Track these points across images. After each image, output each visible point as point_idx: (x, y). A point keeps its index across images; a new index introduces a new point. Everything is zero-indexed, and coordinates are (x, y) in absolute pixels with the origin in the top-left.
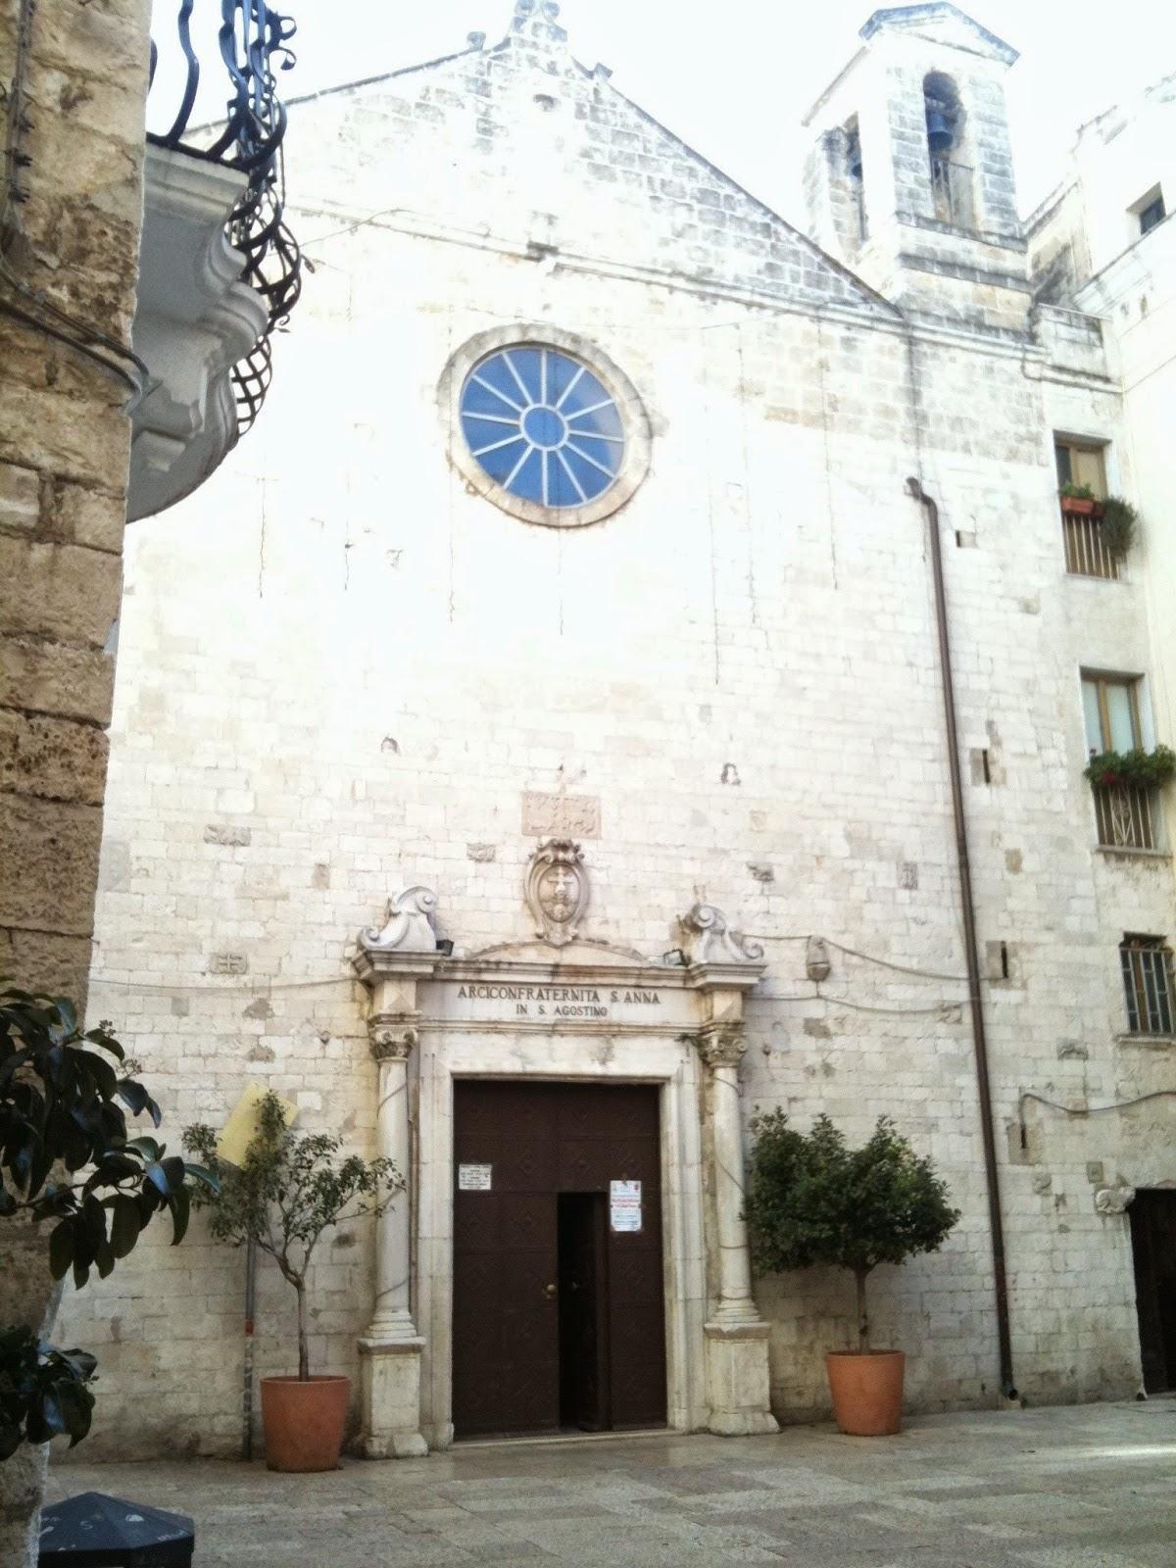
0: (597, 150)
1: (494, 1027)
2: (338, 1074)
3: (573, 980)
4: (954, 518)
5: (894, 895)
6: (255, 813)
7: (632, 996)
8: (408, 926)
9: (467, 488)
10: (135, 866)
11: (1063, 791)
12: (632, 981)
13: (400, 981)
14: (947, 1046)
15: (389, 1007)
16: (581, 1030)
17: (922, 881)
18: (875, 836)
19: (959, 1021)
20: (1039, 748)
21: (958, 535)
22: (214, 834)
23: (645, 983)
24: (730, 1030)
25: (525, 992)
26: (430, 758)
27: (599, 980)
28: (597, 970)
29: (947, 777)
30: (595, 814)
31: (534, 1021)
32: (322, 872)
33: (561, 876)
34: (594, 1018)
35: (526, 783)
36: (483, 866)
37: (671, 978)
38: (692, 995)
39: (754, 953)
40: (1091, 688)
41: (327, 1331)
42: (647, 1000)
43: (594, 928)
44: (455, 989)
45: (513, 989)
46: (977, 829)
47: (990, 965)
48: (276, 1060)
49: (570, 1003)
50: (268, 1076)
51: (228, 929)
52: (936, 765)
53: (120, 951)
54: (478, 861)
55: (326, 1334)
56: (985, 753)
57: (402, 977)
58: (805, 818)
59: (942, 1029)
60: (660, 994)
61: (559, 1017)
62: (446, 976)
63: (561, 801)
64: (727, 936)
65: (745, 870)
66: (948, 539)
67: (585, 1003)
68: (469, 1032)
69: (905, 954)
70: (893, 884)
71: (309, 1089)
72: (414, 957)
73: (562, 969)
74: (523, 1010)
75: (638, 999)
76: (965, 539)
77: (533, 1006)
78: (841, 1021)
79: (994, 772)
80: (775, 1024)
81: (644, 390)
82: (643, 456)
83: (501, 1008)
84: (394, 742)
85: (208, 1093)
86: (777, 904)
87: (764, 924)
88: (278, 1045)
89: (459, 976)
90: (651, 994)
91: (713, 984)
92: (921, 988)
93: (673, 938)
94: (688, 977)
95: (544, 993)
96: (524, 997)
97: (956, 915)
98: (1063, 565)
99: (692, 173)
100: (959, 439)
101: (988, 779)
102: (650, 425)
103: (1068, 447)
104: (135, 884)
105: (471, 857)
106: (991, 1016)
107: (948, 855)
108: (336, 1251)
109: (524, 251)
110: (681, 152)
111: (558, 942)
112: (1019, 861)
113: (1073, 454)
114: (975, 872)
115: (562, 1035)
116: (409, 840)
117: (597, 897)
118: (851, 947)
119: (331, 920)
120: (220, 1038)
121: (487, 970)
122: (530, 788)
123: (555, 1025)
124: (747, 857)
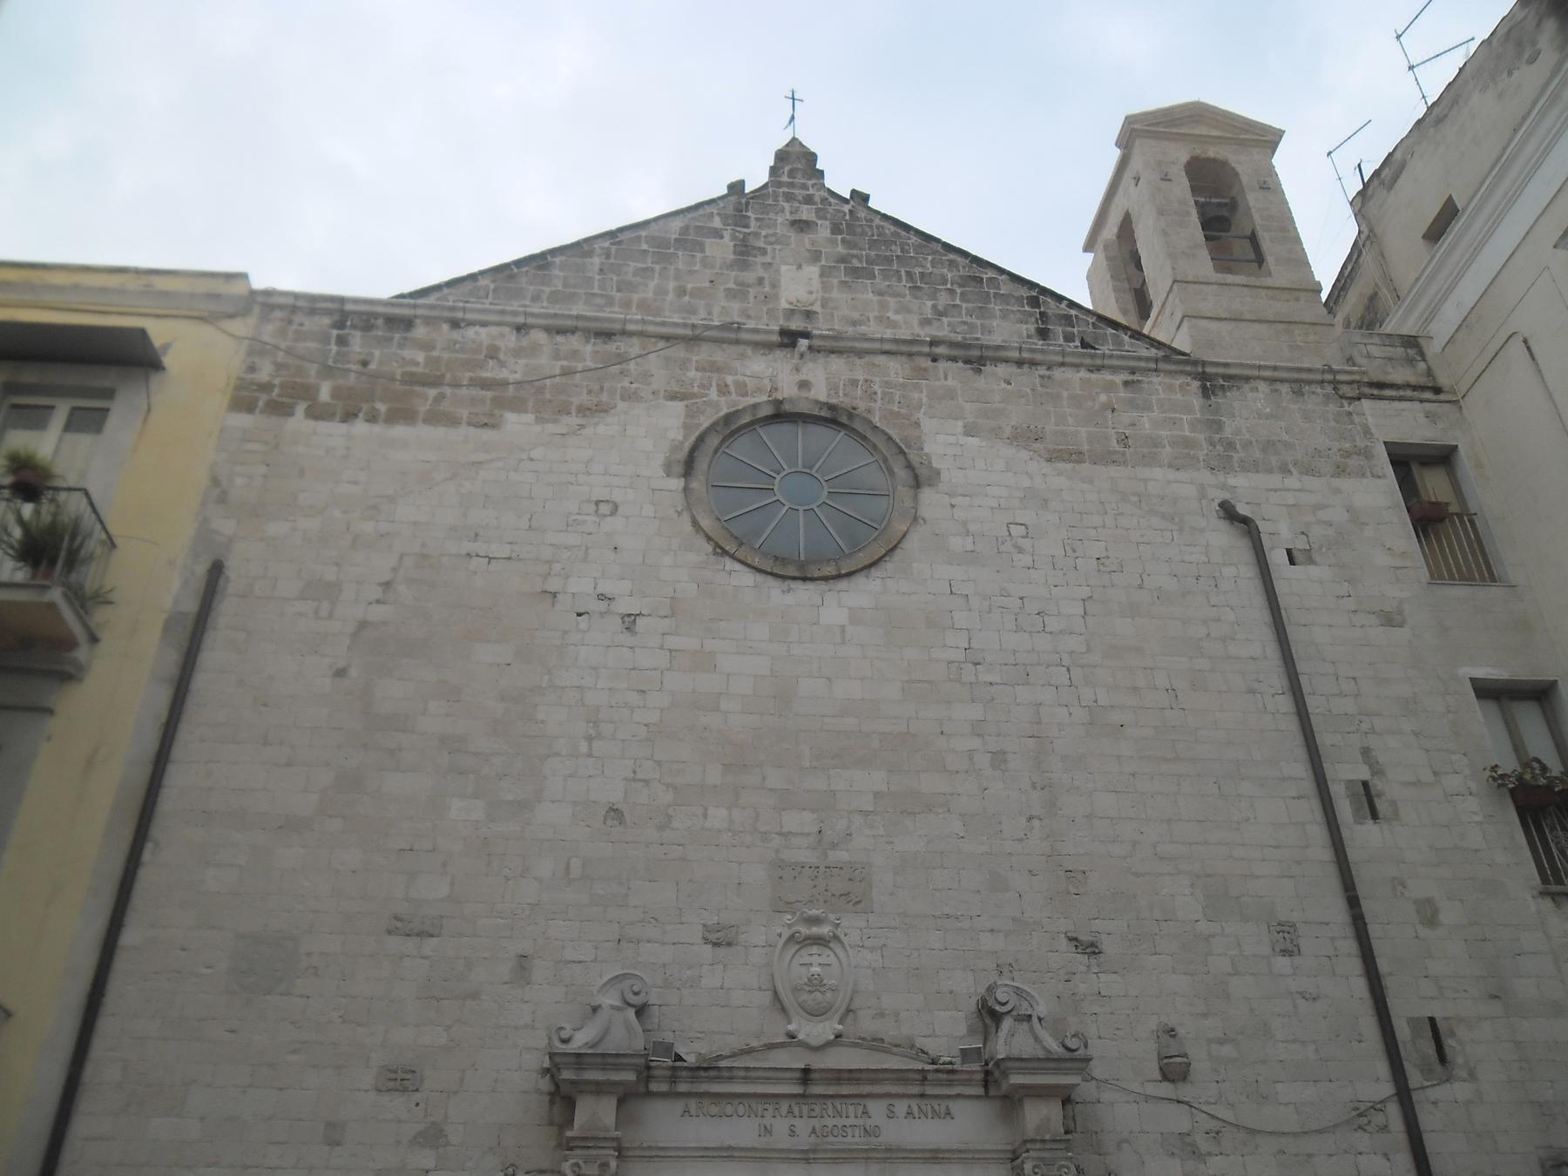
0: (853, 256)
3: (831, 1090)
4: (1279, 533)
7: (915, 1109)
9: (714, 549)
11: (1481, 823)
12: (915, 1090)
19: (1384, 1128)
20: (1435, 774)
21: (1289, 552)
22: (399, 924)
23: (929, 1090)
27: (867, 1089)
28: (864, 1076)
29: (1319, 815)
31: (780, 1146)
34: (863, 1140)
35: (777, 851)
36: (722, 951)
37: (967, 1083)
39: (1073, 1044)
40: (1492, 706)
42: (936, 1114)
46: (1364, 877)
47: (1415, 1048)
49: (830, 1122)
54: (716, 945)
56: (1365, 784)
57: (599, 1089)
58: (1137, 875)
59: (1362, 1140)
60: (957, 1107)
62: (664, 1087)
65: (1064, 941)
66: (1277, 558)
67: (852, 1121)
69: (1294, 1041)
72: (610, 1060)
74: (767, 1130)
76: (1298, 556)
77: (780, 1126)
79: (1381, 806)
81: (909, 447)
82: (908, 503)
90: (941, 1106)
91: (1023, 1086)
93: (971, 1031)
94: (988, 1080)
95: (796, 1110)
96: (768, 1114)
98: (1424, 573)
99: (952, 263)
100: (1274, 460)
101: (1375, 815)
102: (916, 477)
103: (1406, 461)
105: (706, 941)
106: (1428, 1120)
107: (1338, 912)
109: (775, 338)
110: (939, 248)
112: (1435, 912)
113: (1415, 469)
114: (1374, 930)
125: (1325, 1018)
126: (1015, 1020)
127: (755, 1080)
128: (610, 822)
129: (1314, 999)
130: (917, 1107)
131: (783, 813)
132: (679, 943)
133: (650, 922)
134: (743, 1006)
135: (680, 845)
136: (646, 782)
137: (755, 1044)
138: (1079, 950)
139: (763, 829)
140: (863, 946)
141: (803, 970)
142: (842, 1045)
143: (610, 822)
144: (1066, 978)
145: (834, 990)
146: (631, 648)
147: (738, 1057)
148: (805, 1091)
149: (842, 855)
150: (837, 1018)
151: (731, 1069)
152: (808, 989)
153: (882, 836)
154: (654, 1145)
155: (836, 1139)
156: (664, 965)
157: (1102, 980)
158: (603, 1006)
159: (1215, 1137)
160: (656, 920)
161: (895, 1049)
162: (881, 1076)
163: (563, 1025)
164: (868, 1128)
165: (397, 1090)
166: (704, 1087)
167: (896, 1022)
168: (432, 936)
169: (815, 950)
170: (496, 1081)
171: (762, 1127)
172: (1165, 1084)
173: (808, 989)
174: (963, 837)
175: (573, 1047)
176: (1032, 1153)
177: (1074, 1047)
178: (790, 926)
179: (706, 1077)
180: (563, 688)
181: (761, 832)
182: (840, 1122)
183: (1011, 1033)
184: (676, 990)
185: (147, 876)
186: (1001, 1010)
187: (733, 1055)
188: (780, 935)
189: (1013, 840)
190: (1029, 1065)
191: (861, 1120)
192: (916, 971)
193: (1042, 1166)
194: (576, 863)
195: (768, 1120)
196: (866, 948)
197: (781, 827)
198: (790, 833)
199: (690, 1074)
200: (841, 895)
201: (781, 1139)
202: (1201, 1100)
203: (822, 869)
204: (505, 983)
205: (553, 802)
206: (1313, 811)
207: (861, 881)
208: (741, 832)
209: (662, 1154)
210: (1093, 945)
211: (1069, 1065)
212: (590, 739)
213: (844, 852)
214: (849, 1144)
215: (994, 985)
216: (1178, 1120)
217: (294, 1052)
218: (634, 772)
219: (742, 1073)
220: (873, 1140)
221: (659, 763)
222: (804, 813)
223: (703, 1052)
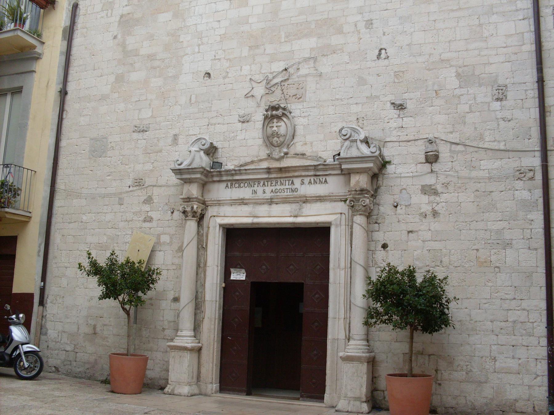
1: (242, 202)
2: (177, 227)
5: (489, 106)
6: (152, 117)
10: (109, 146)
12: (312, 173)
14: (525, 194)
16: (286, 201)
17: (510, 95)
18: (477, 73)
19: (532, 179)
22: (136, 129)
24: (359, 194)
25: (257, 184)
31: (260, 197)
32: (175, 138)
33: (275, 123)
34: (291, 194)
37: (333, 169)
41: (168, 338)
42: (321, 182)
43: (298, 148)
44: (223, 185)
45: (250, 182)
48: (154, 222)
50: (150, 228)
51: (139, 167)
52: (526, 22)
53: (102, 181)
54: (243, 122)
55: (167, 339)
60: (329, 179)
61: (273, 194)
62: (216, 179)
65: (389, 104)
67: (287, 187)
68: (240, 204)
69: (494, 141)
70: (489, 99)
71: (165, 234)
73: (272, 170)
74: (255, 192)
75: (315, 182)
77: (260, 190)
78: (446, 185)
80: (401, 190)
83: (245, 192)
84: (209, 74)
85: (129, 236)
86: (407, 121)
87: (399, 134)
88: (155, 215)
89: (224, 178)
92: (504, 161)
95: (266, 183)
96: (256, 186)
97: (535, 113)
104: (109, 153)
105: (240, 121)
107: (531, 76)
108: (172, 304)
111: (277, 157)
115: (277, 204)
117: (300, 131)
118: (457, 141)
120: (134, 213)
121: (236, 174)
123: (271, 199)
124: (391, 98)
125: (513, 129)
126: (351, 142)
127: (249, 174)
129: (509, 120)
130: (313, 180)
131: (272, 64)
132: (229, 123)
134: (252, 145)
135: (231, 84)
136: (219, 59)
138: (396, 108)
140: (300, 116)
142: (289, 158)
143: (206, 78)
144: (388, 121)
145: (285, 136)
146: (215, 3)
151: (246, 170)
157: (404, 121)
159: (446, 186)
160: (221, 115)
162: (297, 169)
165: (138, 186)
168: (146, 131)
170: (167, 180)
171: (253, 191)
172: (427, 164)
174: (348, 63)
180: (190, 26)
181: (262, 73)
185: (65, 123)
196: (302, 117)
197: (271, 70)
199: (226, 173)
200: (293, 96)
201: (260, 194)
202: (442, 170)
204: (170, 145)
205: (186, 74)
206: (530, 25)
207: (302, 89)
210: (401, 105)
212: (199, 45)
216: (430, 180)
217: (109, 176)
218: (215, 56)
219: (244, 172)
220: (295, 193)
221: (224, 51)
222: (281, 62)
223: (236, 164)
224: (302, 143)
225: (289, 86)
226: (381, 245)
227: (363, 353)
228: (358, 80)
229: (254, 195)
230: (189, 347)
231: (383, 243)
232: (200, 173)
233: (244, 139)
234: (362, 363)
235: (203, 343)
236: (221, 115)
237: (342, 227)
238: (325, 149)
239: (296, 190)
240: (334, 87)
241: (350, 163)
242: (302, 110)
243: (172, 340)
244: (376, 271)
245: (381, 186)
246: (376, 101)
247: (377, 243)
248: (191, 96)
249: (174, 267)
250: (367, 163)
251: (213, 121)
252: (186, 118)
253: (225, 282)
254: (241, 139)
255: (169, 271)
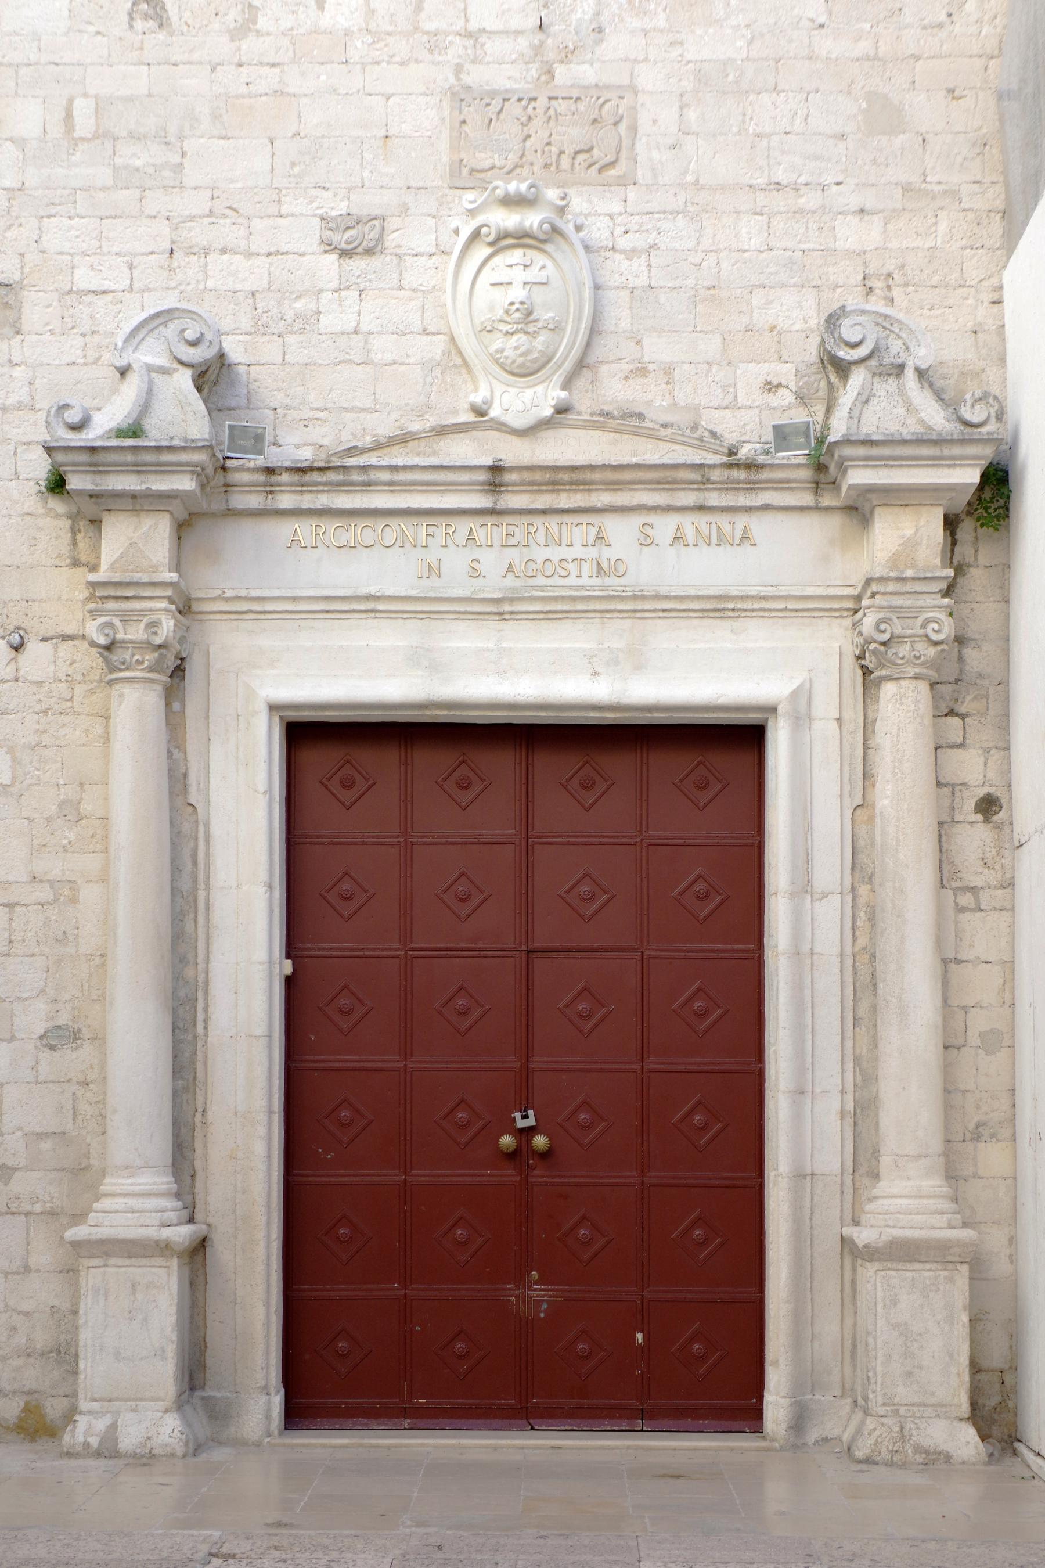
2: (45, 712)
3: (543, 501)
8: (150, 392)
12: (689, 498)
13: (136, 511)
15: (112, 568)
23: (713, 499)
26: (238, 33)
30: (623, 127)
34: (598, 582)
35: (458, 69)
36: (357, 265)
37: (781, 485)
38: (836, 521)
39: (975, 415)
54: (345, 254)
60: (759, 526)
62: (254, 501)
63: (542, 102)
64: (909, 373)
67: (578, 551)
73: (508, 477)
105: (329, 247)
108: (45, 1055)
116: (192, 218)
119: (26, 399)
122: (467, 80)
126: (874, 375)
128: (139, 25)
133: (224, 216)
137: (415, 427)
139: (430, 26)
140: (613, 249)
141: (497, 293)
143: (139, 25)
147: (386, 450)
148: (495, 503)
149: (585, 72)
150: (558, 378)
151: (365, 469)
152: (505, 328)
153: (661, 31)
154: (243, 593)
155: (550, 582)
156: (253, 294)
158: (134, 366)
160: (235, 210)
161: (663, 432)
163: (68, 401)
164: (605, 565)
166: (324, 500)
167: (668, 383)
169: (516, 256)
171: (425, 564)
173: (505, 328)
175: (90, 436)
176: (879, 600)
177: (975, 419)
178: (472, 213)
179: (325, 484)
181: (427, 33)
182: (556, 553)
183: (864, 398)
184: (275, 337)
186: (848, 358)
187: (378, 446)
188: (457, 232)
189: (924, 28)
190: (886, 451)
191: (595, 549)
192: (712, 292)
193: (895, 620)
194: (83, 109)
195: (432, 555)
197: (467, 20)
198: (483, 31)
199: (296, 478)
200: (577, 153)
203: (542, 102)
208: (389, 34)
209: (256, 607)
211: (957, 450)
213: (586, 66)
214: (570, 588)
215: (839, 312)
219: (385, 476)
220: (612, 581)
223: (325, 442)
224: (625, 367)
225: (553, 102)
226: (973, 802)
227: (951, 1227)
228: (864, 105)
229: (425, 582)
230: (177, 1239)
231: (982, 792)
232: (192, 472)
233: (356, 332)
234: (950, 1266)
235: (210, 1220)
236: (235, 210)
237: (814, 726)
238: (729, 398)
239: (618, 569)
240: (759, 130)
241: (886, 466)
242: (619, 220)
243: (79, 1217)
244: (957, 904)
245: (969, 566)
246: (942, 208)
247: (958, 794)
248: (70, 101)
249: (44, 893)
250: (954, 466)
251: (198, 234)
252: (52, 210)
253: (288, 956)
254: (338, 329)
255: (18, 909)
